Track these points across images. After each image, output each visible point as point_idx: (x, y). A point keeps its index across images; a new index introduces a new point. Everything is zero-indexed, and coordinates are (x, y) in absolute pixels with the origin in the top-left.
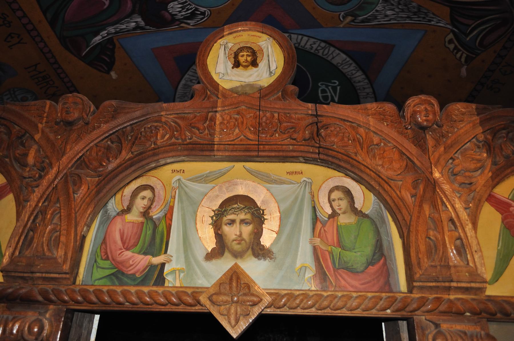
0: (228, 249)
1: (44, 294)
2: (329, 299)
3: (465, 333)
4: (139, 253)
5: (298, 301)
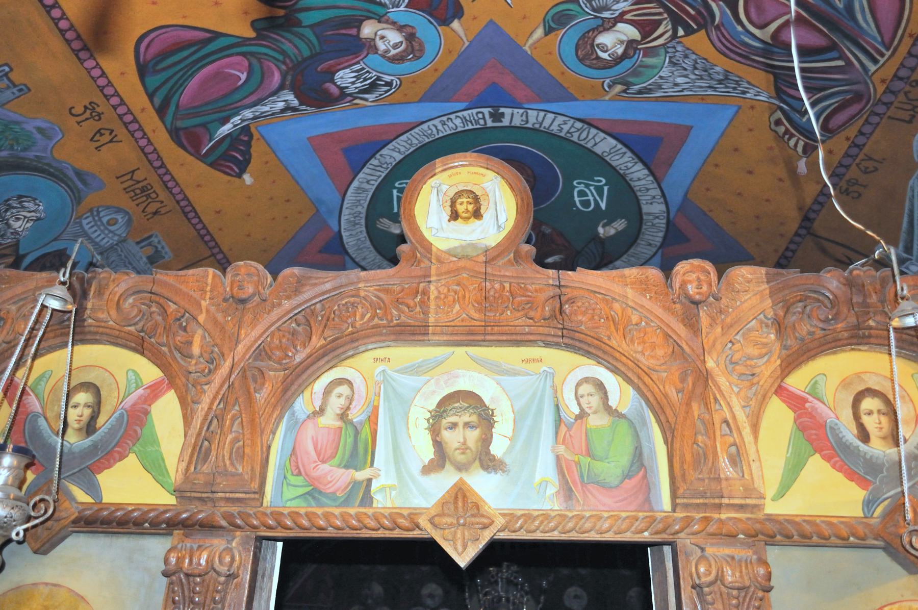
0: (450, 460)
1: (228, 517)
2: (574, 521)
3: (733, 558)
4: (339, 466)
5: (536, 523)
